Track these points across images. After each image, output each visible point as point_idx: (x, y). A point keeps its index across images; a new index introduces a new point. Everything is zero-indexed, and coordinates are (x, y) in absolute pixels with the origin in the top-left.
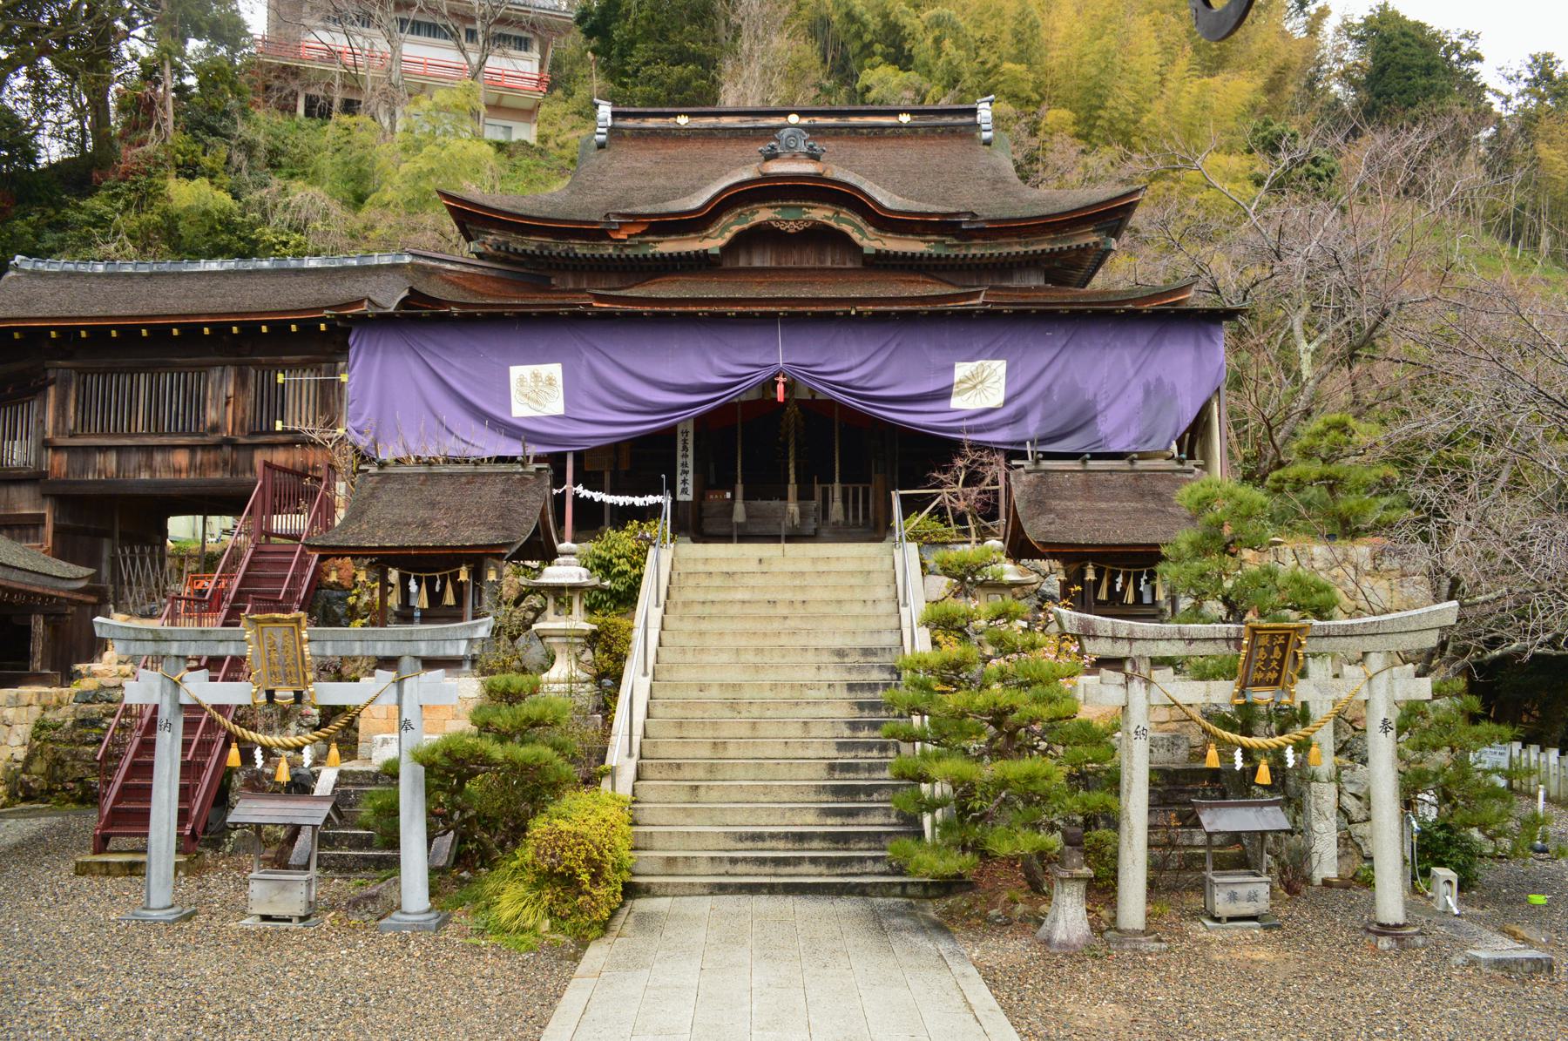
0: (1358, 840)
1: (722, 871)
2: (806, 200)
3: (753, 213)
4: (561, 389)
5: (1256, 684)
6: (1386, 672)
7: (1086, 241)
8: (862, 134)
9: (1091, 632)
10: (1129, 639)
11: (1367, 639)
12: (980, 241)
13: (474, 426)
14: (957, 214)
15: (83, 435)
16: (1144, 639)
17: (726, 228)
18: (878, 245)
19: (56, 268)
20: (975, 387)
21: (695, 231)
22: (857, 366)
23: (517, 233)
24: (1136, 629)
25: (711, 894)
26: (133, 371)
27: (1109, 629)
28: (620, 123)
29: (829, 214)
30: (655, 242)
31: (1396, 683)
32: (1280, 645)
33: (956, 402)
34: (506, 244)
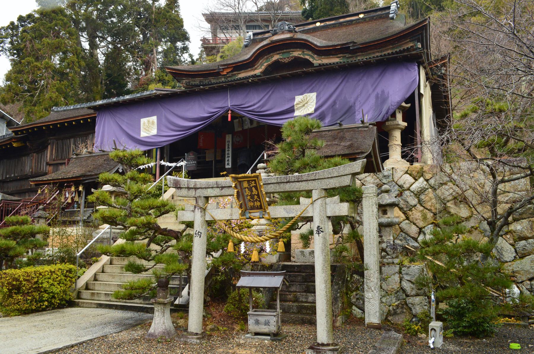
0: (410, 305)
1: (108, 299)
2: (290, 48)
3: (272, 57)
4: (156, 125)
5: (253, 208)
6: (319, 200)
7: (407, 46)
8: (344, 25)
9: (179, 186)
10: (195, 188)
11: (310, 183)
12: (361, 54)
13: (130, 142)
14: (347, 44)
15: (57, 160)
16: (201, 188)
17: (262, 64)
18: (320, 62)
19: (62, 109)
20: (304, 105)
21: (250, 67)
22: (257, 103)
23: (192, 78)
24: (198, 183)
25: (97, 308)
26: (70, 138)
27: (186, 184)
28: (256, 37)
29: (300, 53)
30: (238, 74)
31: (328, 206)
32: (254, 186)
33: (297, 113)
34: (189, 82)
